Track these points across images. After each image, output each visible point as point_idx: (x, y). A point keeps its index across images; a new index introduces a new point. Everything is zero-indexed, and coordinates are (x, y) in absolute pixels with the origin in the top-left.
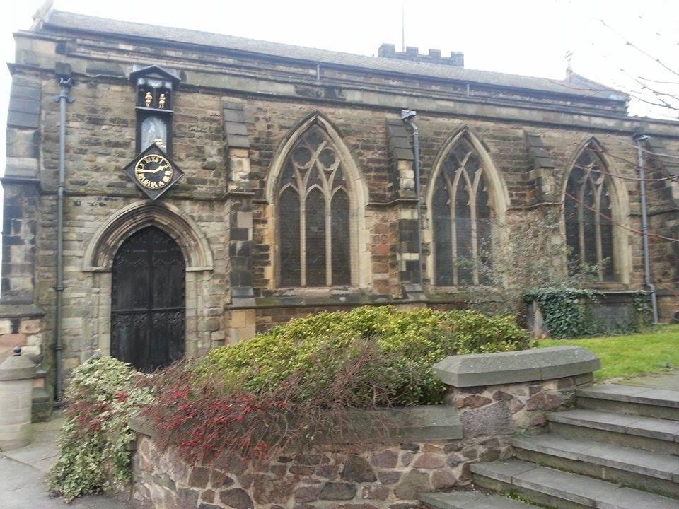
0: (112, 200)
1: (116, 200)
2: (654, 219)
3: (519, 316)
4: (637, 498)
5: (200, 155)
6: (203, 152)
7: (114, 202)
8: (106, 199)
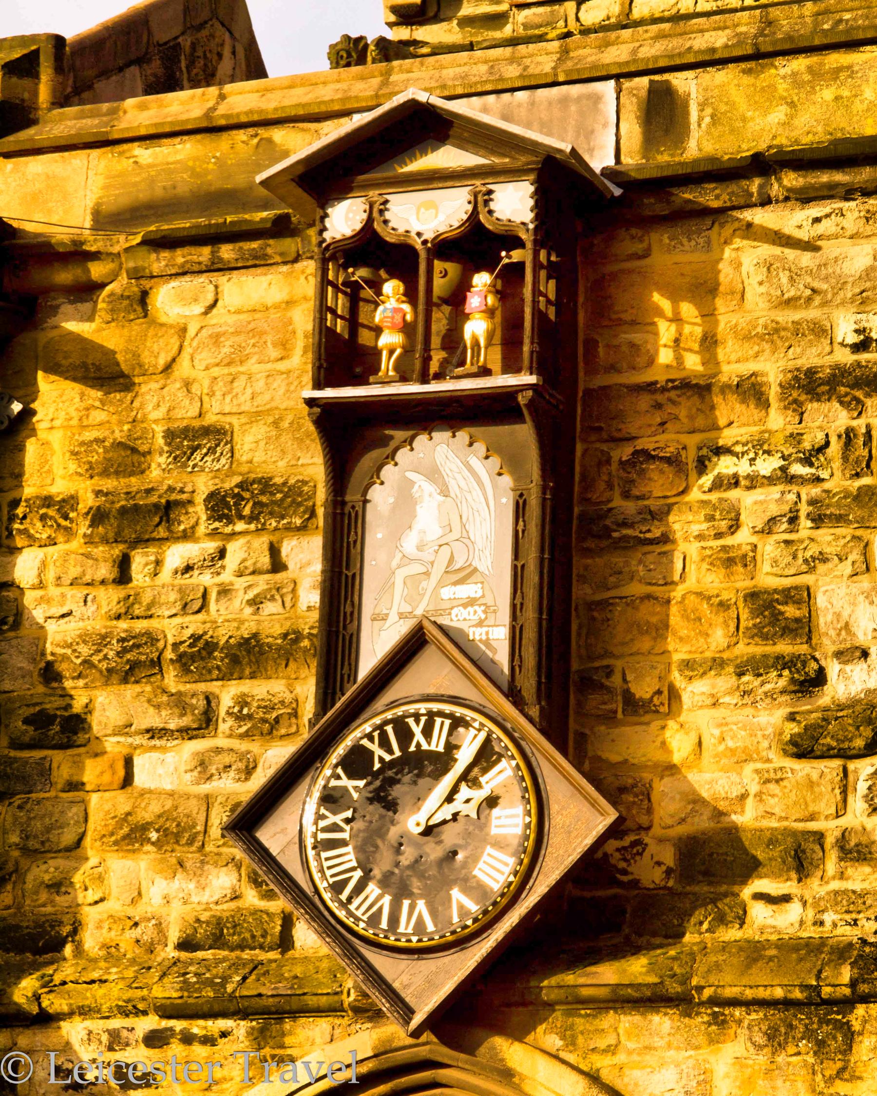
0: (188, 1039)
1: (208, 1040)
2: (202, 703)
3: (841, 403)
4: (726, 157)
5: (784, 647)
6: (804, 628)
7: (200, 1051)
8: (154, 1040)
